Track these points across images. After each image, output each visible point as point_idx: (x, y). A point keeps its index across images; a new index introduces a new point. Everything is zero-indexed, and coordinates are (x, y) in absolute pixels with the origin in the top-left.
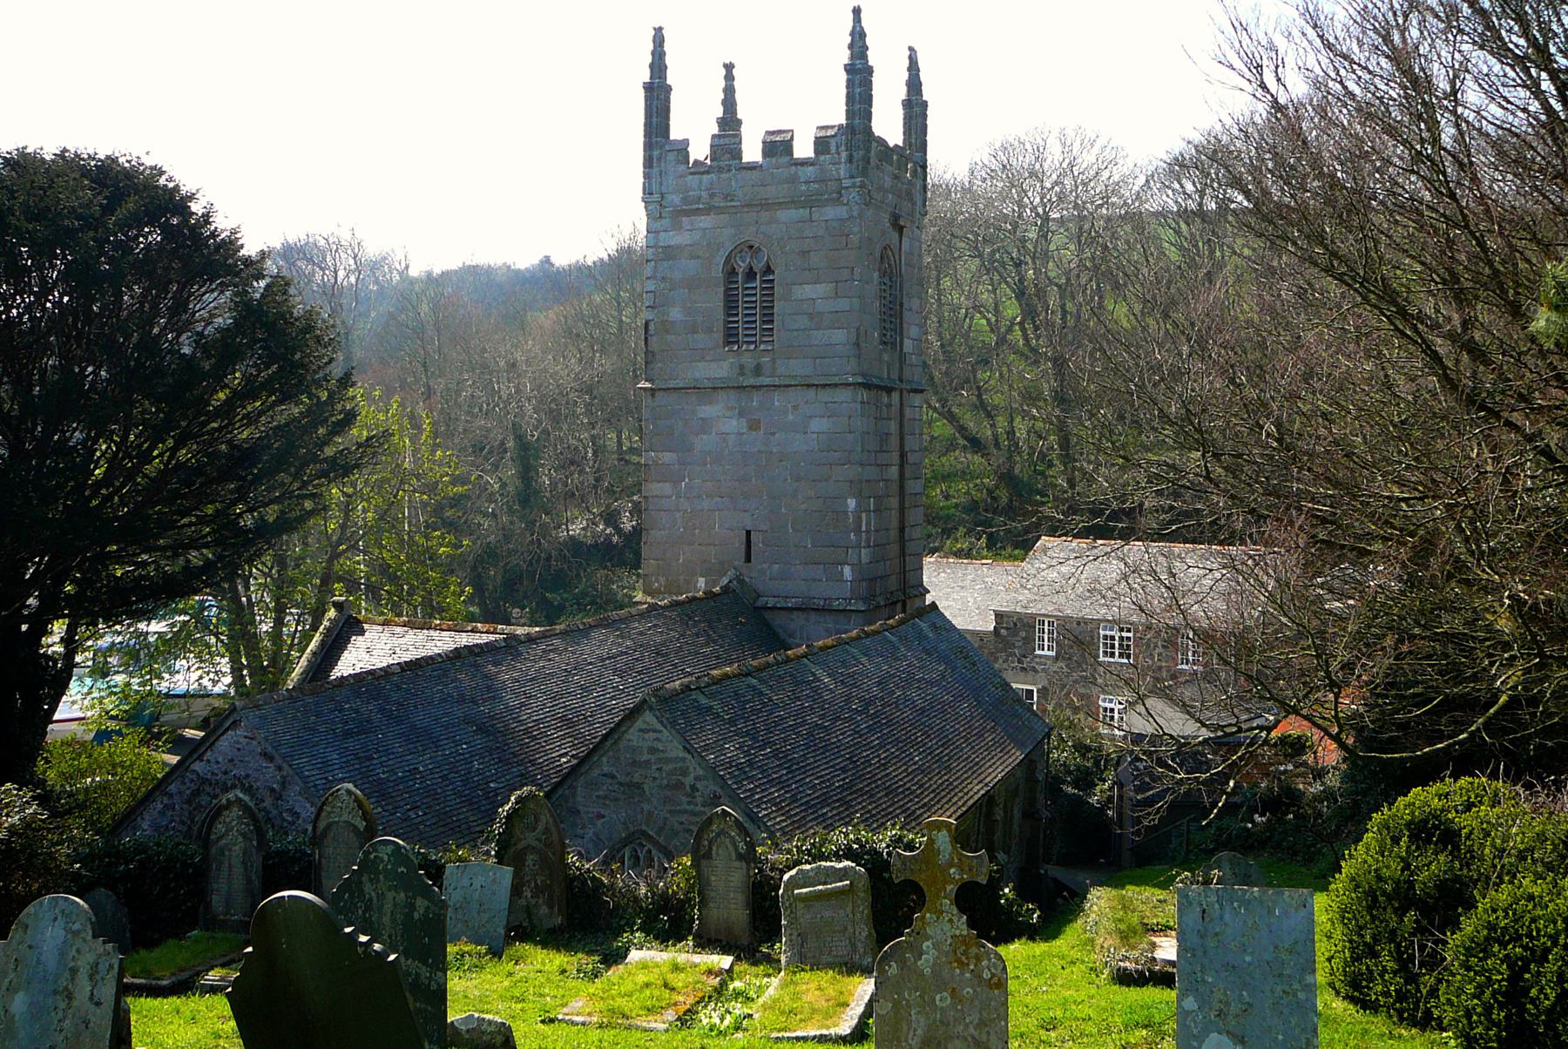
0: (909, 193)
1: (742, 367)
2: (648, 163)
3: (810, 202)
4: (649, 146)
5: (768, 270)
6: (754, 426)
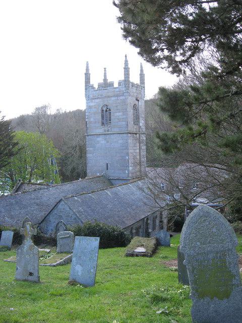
0: (140, 93)
1: (105, 130)
2: (86, 89)
3: (117, 96)
4: (86, 86)
5: (110, 110)
6: (108, 142)
